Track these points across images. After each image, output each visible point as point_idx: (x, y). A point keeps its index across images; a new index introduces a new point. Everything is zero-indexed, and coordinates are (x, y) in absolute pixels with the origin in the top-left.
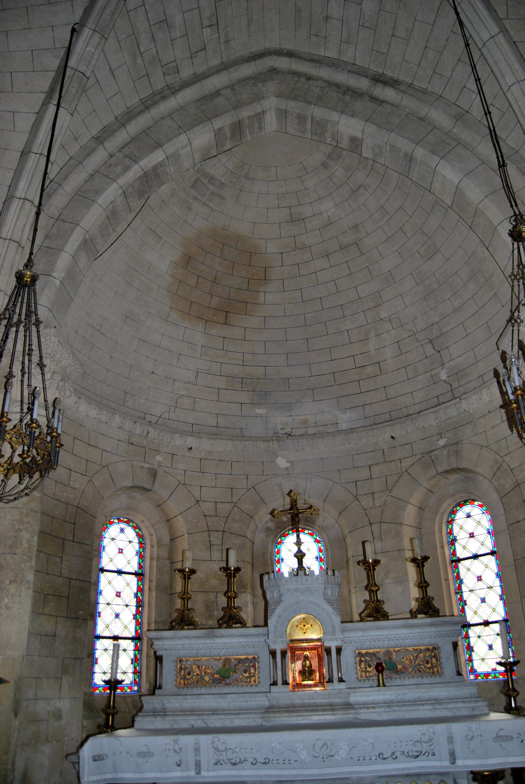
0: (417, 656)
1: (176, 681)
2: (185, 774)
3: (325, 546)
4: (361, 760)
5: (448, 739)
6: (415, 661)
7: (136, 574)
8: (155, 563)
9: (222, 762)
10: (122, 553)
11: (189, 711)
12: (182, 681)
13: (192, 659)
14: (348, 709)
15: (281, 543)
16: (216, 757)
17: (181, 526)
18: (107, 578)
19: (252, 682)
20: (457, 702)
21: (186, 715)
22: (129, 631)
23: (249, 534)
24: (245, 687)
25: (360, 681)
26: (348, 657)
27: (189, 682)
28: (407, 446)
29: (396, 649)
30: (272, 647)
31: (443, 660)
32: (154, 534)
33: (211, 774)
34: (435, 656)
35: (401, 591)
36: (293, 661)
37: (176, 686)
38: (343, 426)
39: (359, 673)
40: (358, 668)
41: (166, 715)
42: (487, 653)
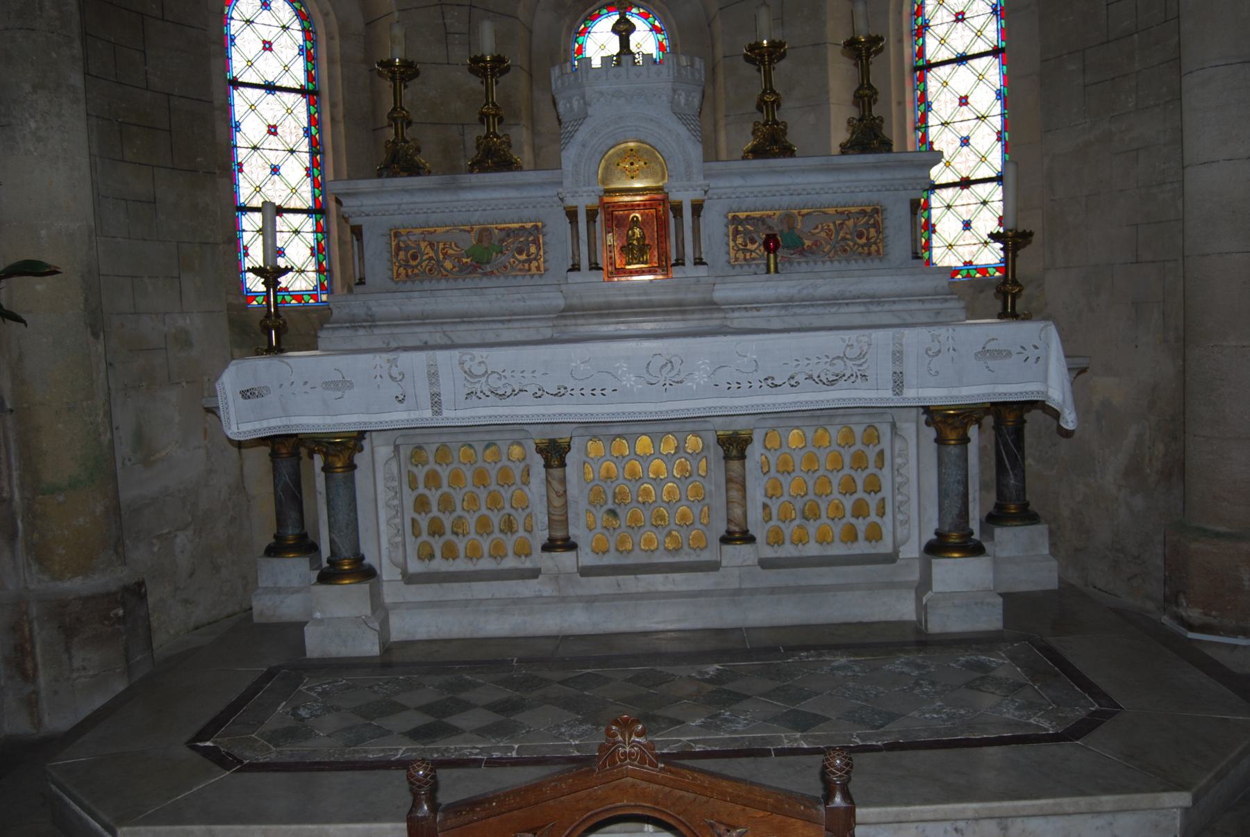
0: (842, 224)
1: (391, 270)
2: (414, 415)
4: (734, 387)
5: (894, 354)
6: (838, 234)
7: (302, 91)
8: (338, 70)
9: (479, 394)
10: (270, 49)
11: (416, 319)
12: (402, 270)
13: (419, 231)
14: (710, 310)
15: (585, 32)
16: (468, 385)
18: (245, 99)
19: (534, 270)
20: (909, 301)
21: (412, 325)
22: (301, 198)
24: (519, 278)
25: (733, 267)
26: (713, 221)
27: (416, 271)
29: (806, 211)
30: (571, 202)
32: (332, 12)
33: (460, 414)
34: (876, 225)
37: (392, 279)
39: (732, 253)
40: (732, 244)
41: (376, 326)
42: (965, 231)
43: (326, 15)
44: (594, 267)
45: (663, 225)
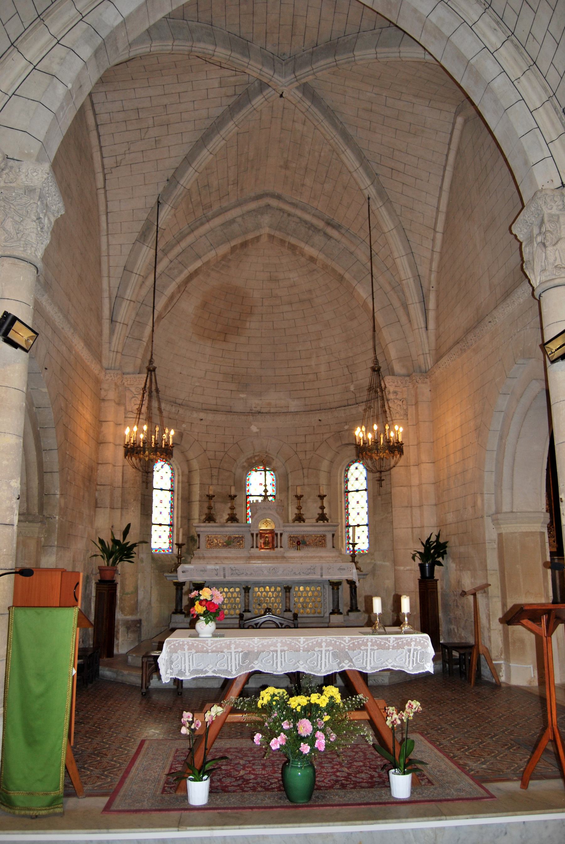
3: (276, 477)
8: (180, 485)
17: (195, 465)
23: (233, 471)
26: (285, 538)
28: (327, 426)
30: (252, 532)
31: (327, 541)
35: (311, 509)
36: (261, 539)
38: (292, 409)
43: (178, 469)
44: (257, 547)
45: (273, 538)
